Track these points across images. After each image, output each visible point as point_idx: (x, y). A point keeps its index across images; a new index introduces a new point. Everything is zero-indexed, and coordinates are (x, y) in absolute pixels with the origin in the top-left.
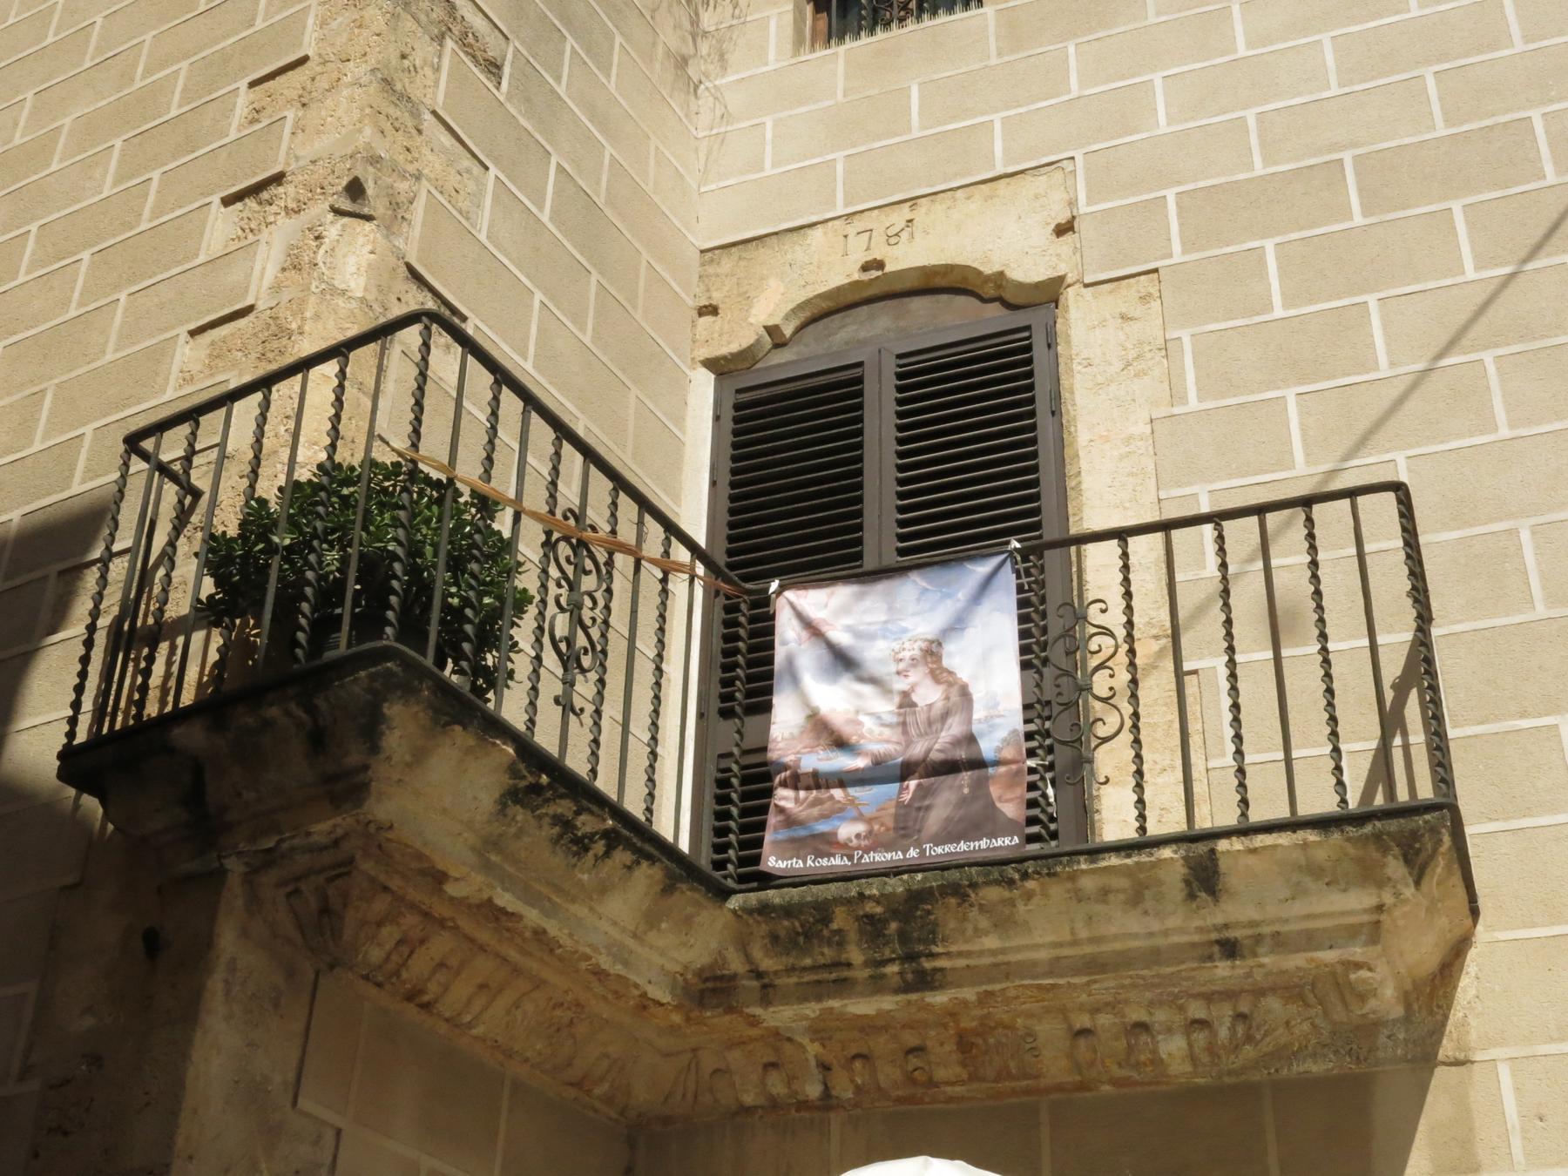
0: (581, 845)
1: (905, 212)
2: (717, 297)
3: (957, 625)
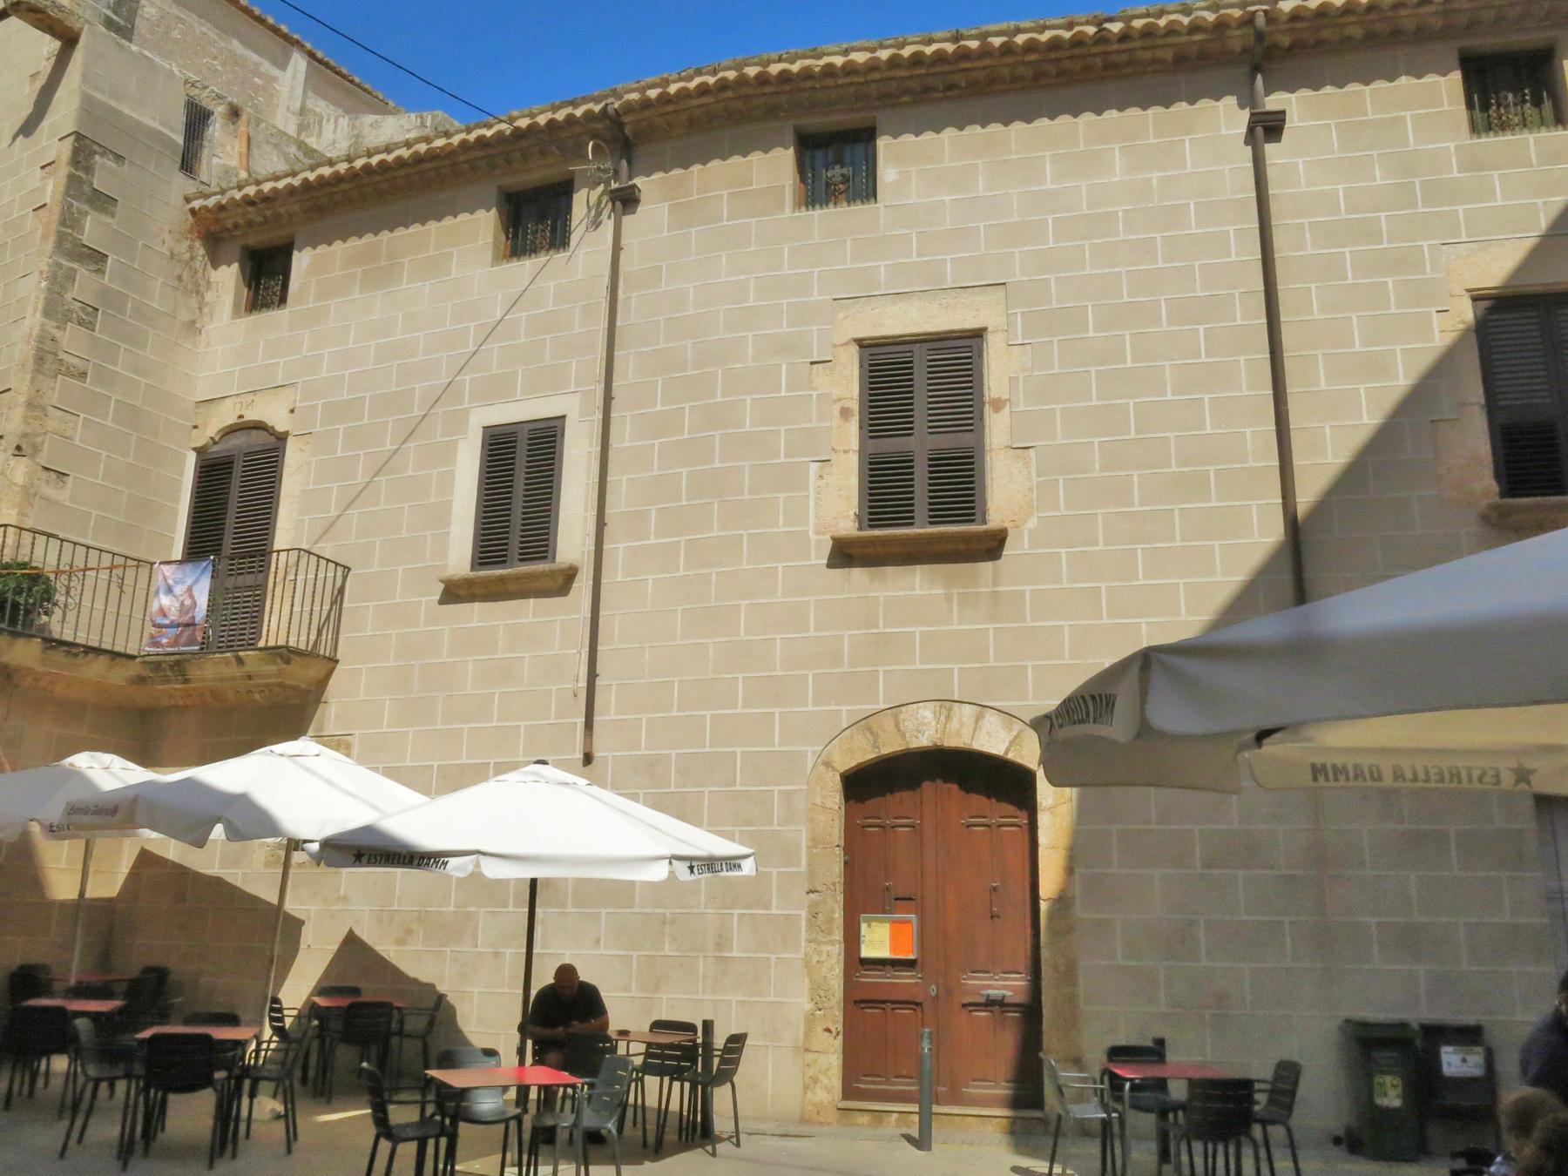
0: (76, 655)
1: (251, 396)
2: (198, 423)
3: (196, 581)
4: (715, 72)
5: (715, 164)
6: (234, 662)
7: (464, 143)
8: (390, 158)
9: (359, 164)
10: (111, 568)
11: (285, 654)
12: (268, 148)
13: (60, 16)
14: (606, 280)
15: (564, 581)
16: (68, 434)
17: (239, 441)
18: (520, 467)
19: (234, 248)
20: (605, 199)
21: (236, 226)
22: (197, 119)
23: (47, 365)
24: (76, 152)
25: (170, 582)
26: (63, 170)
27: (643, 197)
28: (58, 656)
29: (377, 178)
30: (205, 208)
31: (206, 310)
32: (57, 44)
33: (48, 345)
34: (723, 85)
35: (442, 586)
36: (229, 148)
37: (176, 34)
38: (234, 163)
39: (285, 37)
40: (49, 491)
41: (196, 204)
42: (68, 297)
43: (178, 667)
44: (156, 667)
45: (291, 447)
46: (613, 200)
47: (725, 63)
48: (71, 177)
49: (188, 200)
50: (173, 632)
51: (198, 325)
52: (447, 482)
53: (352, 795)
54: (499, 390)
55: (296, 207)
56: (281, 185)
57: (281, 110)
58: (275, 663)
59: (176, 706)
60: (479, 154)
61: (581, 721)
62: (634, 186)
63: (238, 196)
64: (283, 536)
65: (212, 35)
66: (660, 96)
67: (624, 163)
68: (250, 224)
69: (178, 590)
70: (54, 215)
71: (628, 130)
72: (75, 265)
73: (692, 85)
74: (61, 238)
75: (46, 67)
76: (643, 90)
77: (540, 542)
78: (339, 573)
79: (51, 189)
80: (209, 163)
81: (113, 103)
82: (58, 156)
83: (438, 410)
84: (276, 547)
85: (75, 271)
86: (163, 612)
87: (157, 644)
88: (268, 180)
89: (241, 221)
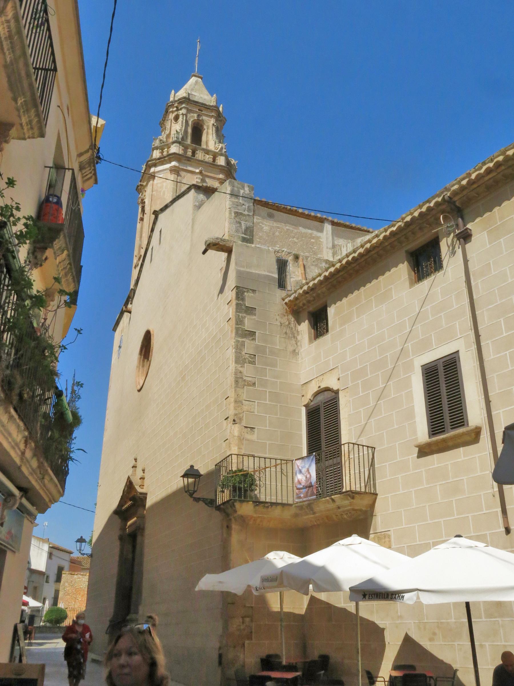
0: (268, 507)
1: (321, 377)
2: (304, 393)
3: (310, 466)
4: (492, 160)
5: (505, 204)
6: (330, 500)
7: (385, 237)
8: (356, 255)
9: (344, 262)
10: (276, 466)
11: (352, 494)
12: (313, 267)
13: (224, 243)
14: (464, 278)
15: (475, 436)
16: (252, 410)
17: (321, 398)
18: (442, 381)
19: (305, 314)
20: (455, 239)
21: (304, 305)
22: (282, 265)
23: (240, 384)
24: (237, 294)
25: (300, 468)
26: (234, 302)
27: (473, 233)
28: (260, 508)
29: (353, 265)
30: (290, 301)
31: (299, 344)
32: (226, 254)
33: (239, 375)
34: (498, 165)
35: (417, 449)
36: (297, 273)
37: (277, 234)
38: (300, 278)
39: (316, 218)
40: (249, 437)
41: (287, 300)
42: (243, 353)
43: (310, 506)
44: (301, 508)
45: (341, 395)
46: (458, 239)
47: (496, 154)
48: (237, 304)
49: (283, 300)
50: (304, 491)
51: (297, 351)
52: (410, 396)
53: (375, 563)
54: (425, 345)
55: (324, 289)
56: (316, 281)
57: (325, 249)
58: (348, 500)
59: (315, 525)
60: (393, 239)
61: (499, 509)
62: (467, 229)
63: (301, 291)
64: (345, 437)
65: (291, 229)
66: (468, 182)
67: (460, 219)
68: (309, 302)
69: (304, 470)
70: (233, 322)
71: (457, 204)
72: (244, 340)
73: (482, 171)
74: (237, 329)
75: (224, 264)
76: (459, 182)
77: (459, 418)
78: (370, 451)
79: (231, 311)
80: (290, 282)
81: (248, 270)
82: (232, 298)
83: (400, 363)
84: (342, 443)
85: (244, 342)
86: (299, 482)
87: (299, 497)
88: (311, 281)
89: (305, 302)
